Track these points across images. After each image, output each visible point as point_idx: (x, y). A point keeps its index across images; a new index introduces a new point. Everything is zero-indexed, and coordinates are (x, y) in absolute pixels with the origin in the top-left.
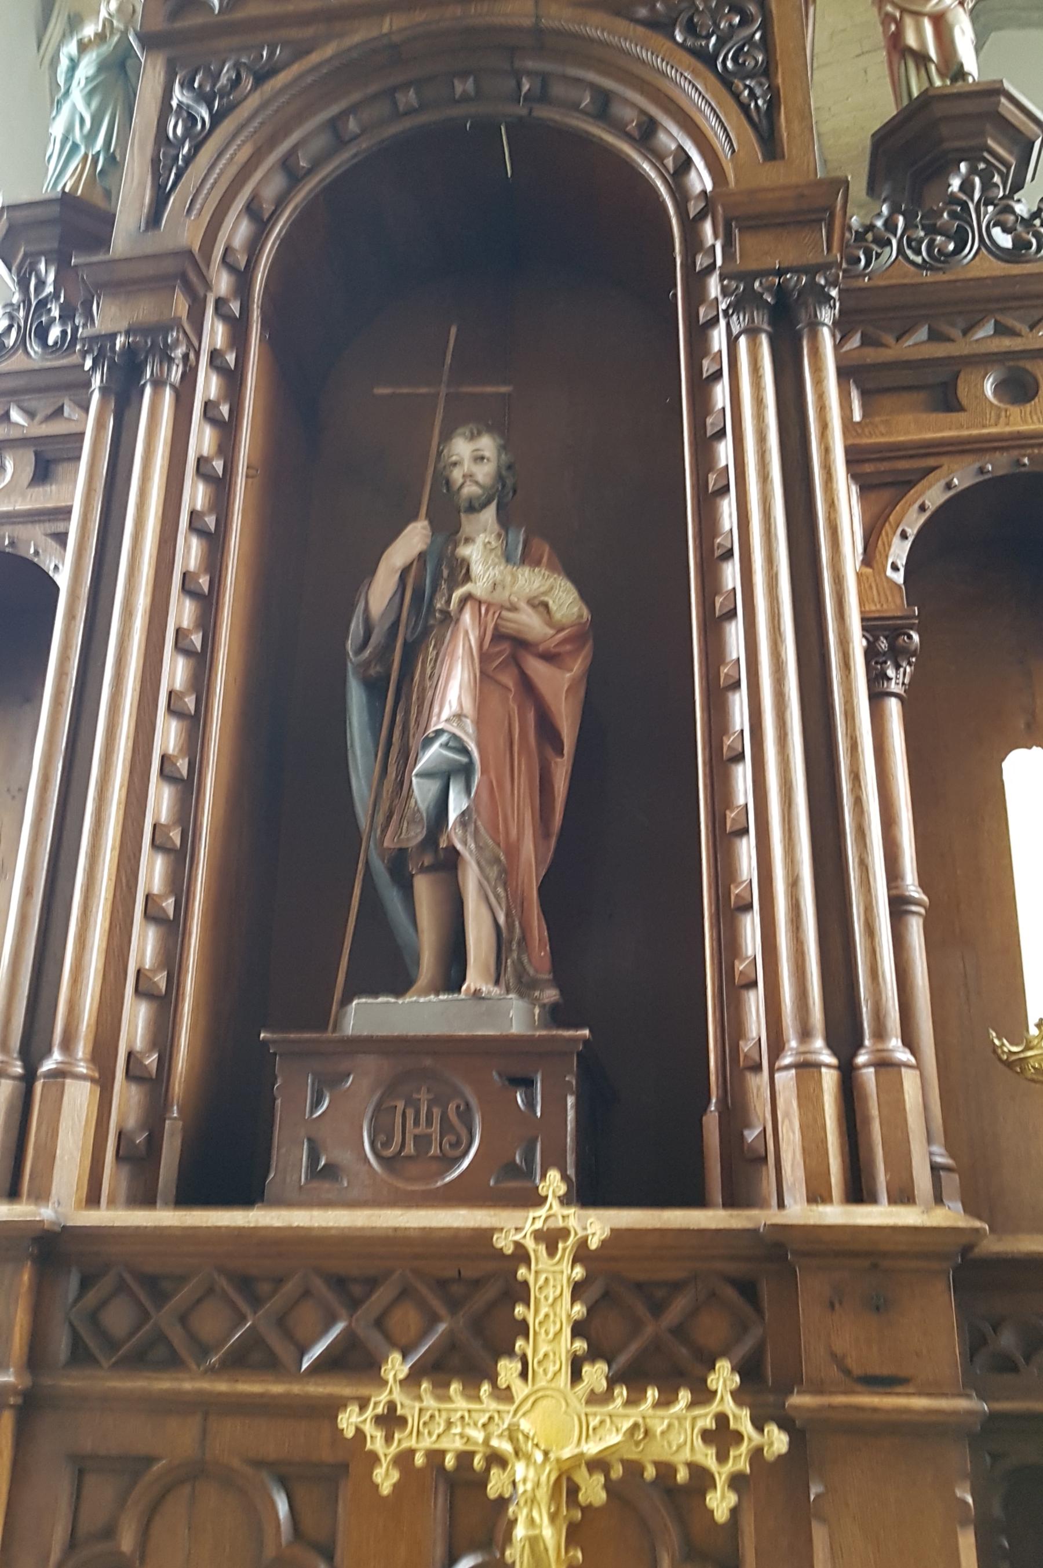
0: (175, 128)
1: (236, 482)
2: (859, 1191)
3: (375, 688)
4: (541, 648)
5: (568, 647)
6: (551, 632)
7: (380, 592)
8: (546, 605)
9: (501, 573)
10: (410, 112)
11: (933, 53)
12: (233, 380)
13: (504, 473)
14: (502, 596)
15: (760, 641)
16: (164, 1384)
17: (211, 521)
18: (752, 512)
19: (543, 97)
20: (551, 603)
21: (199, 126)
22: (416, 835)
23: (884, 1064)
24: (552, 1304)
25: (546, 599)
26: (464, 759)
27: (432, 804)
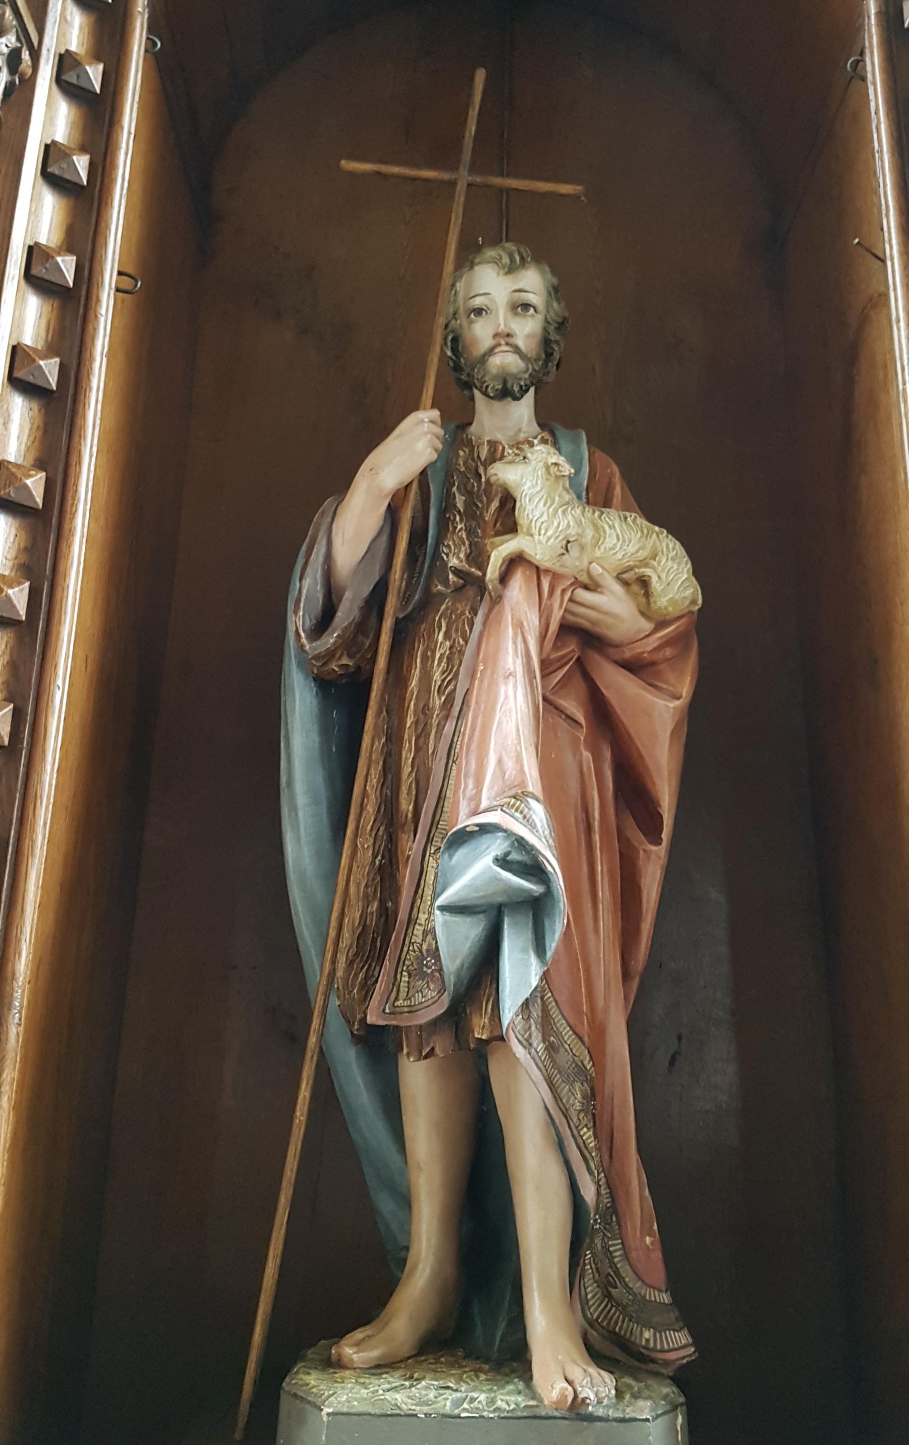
1: (98, 300)
3: (344, 696)
4: (628, 654)
5: (668, 652)
6: (648, 626)
7: (353, 528)
8: (644, 582)
9: (579, 524)
12: (97, 112)
13: (554, 336)
14: (573, 563)
17: (50, 369)
20: (654, 579)
22: (430, 1003)
25: (648, 571)
26: (534, 888)
27: (466, 965)
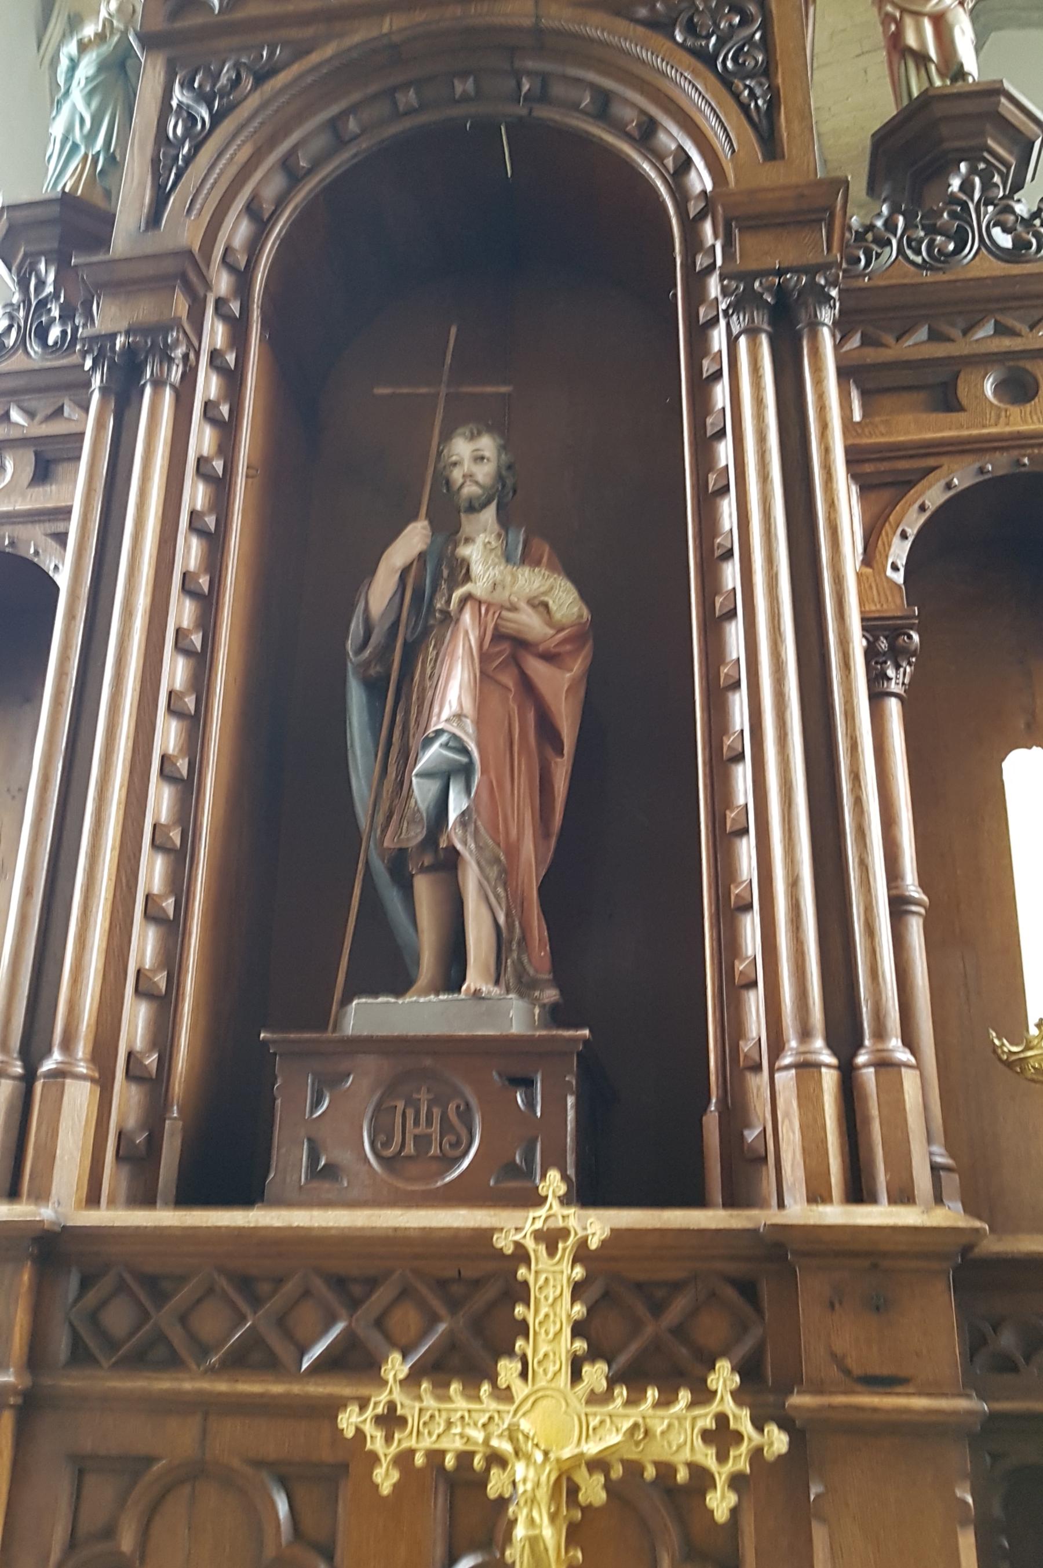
0: (175, 128)
1: (236, 482)
2: (859, 1191)
4: (541, 648)
5: (568, 647)
6: (551, 632)
7: (380, 592)
8: (546, 605)
9: (501, 573)
10: (410, 112)
11: (933, 53)
12: (233, 380)
13: (504, 473)
15: (760, 641)
16: (164, 1384)
17: (211, 521)
18: (752, 512)
19: (543, 97)
20: (551, 603)
21: (199, 126)
22: (416, 835)
23: (884, 1064)
24: (552, 1304)
25: (546, 599)
26: (464, 759)
27: (432, 804)
